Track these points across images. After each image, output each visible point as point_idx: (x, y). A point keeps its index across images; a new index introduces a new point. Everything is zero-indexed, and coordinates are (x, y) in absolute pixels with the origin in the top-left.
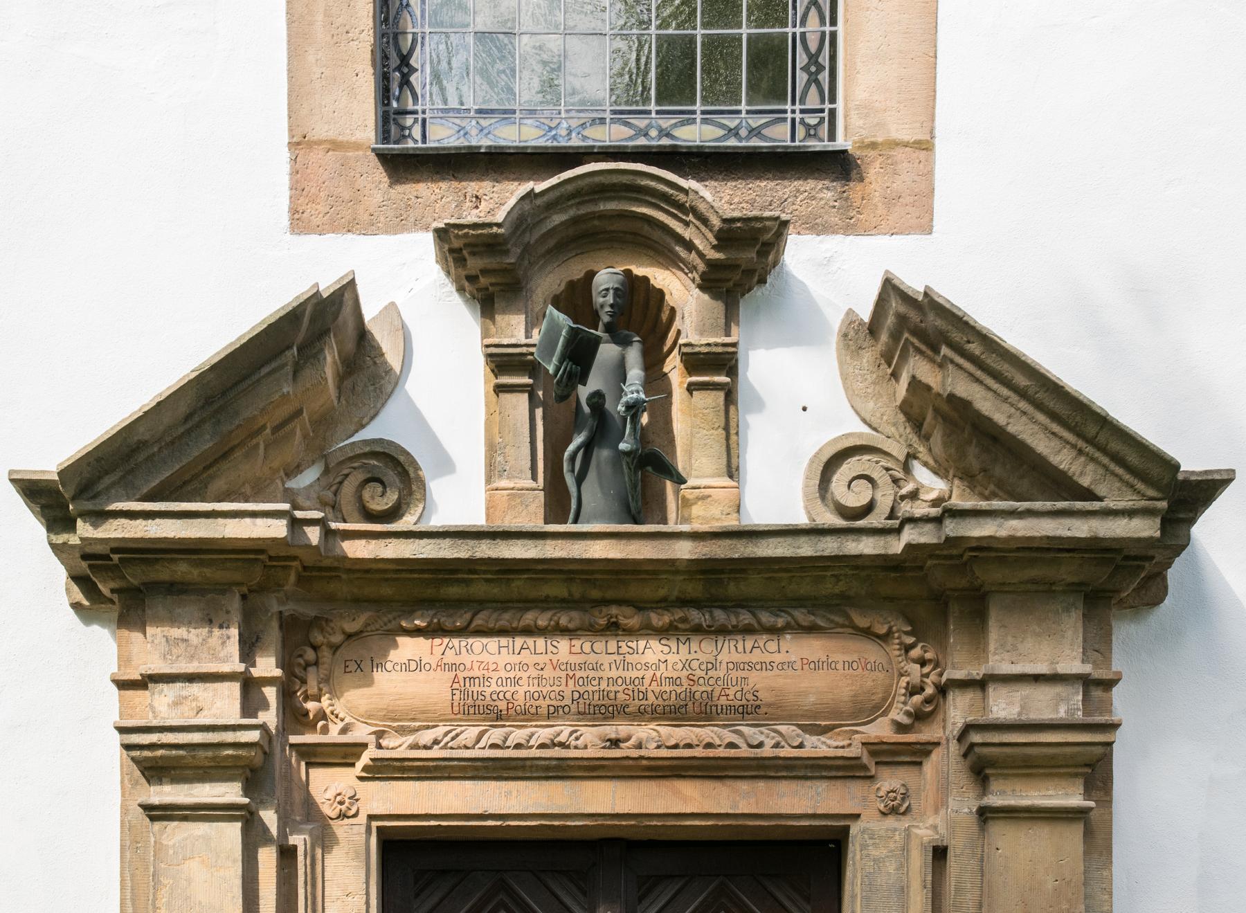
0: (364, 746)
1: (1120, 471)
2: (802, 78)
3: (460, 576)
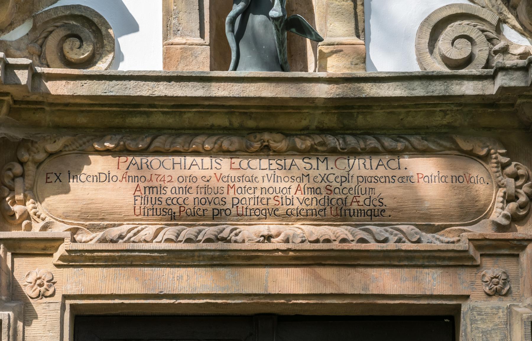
3: (142, 109)
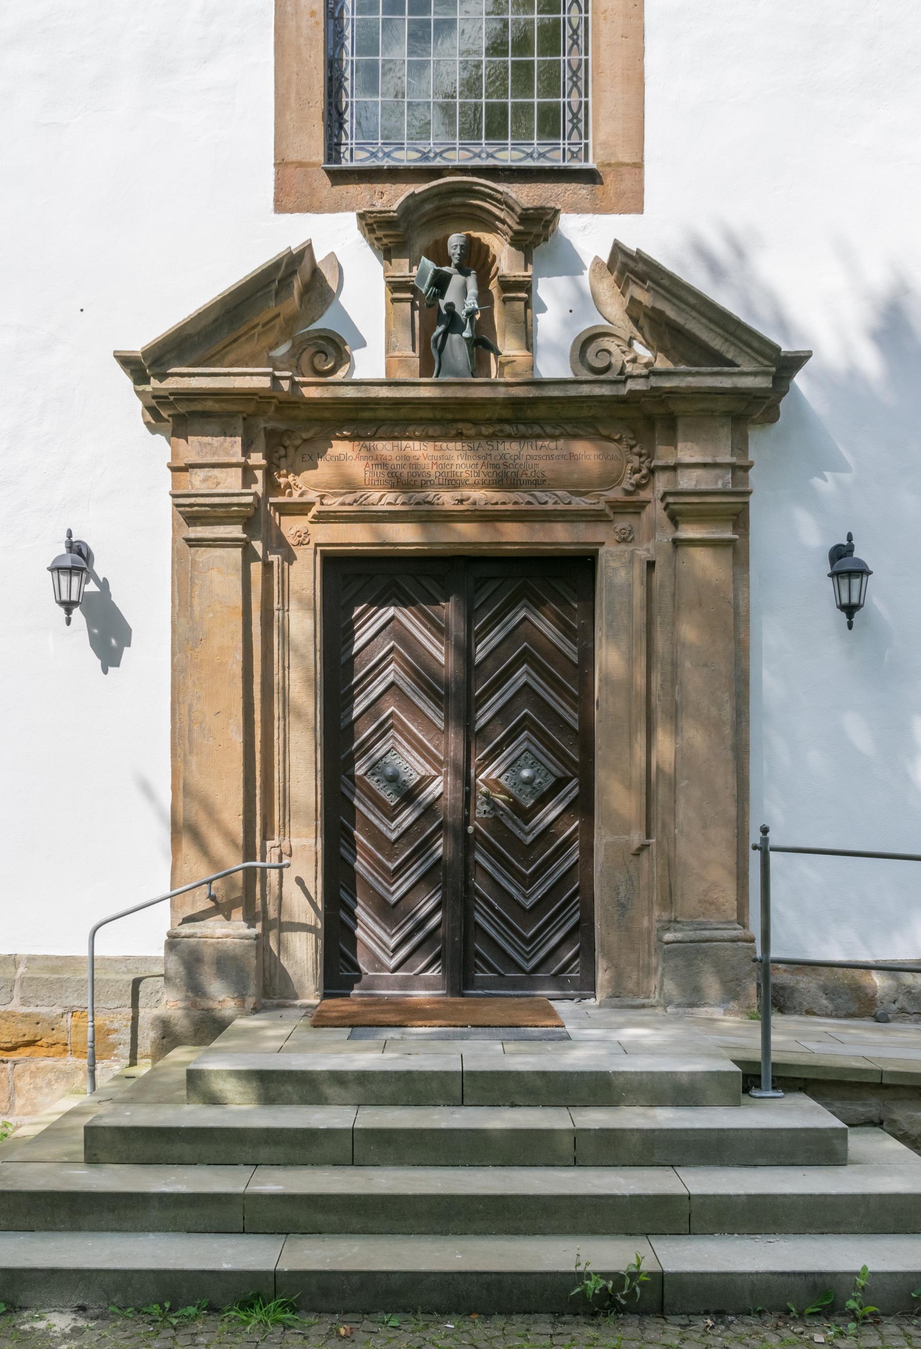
0: (313, 504)
1: (749, 351)
2: (569, 126)
3: (370, 406)
